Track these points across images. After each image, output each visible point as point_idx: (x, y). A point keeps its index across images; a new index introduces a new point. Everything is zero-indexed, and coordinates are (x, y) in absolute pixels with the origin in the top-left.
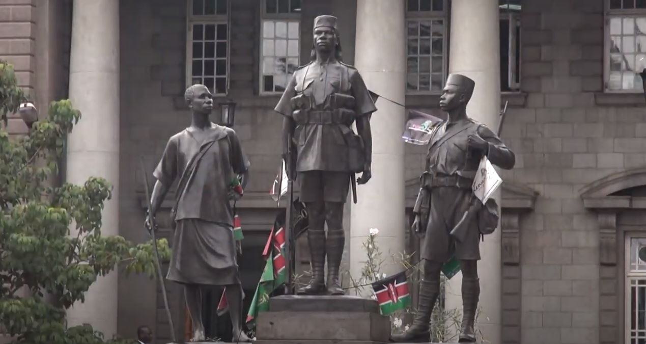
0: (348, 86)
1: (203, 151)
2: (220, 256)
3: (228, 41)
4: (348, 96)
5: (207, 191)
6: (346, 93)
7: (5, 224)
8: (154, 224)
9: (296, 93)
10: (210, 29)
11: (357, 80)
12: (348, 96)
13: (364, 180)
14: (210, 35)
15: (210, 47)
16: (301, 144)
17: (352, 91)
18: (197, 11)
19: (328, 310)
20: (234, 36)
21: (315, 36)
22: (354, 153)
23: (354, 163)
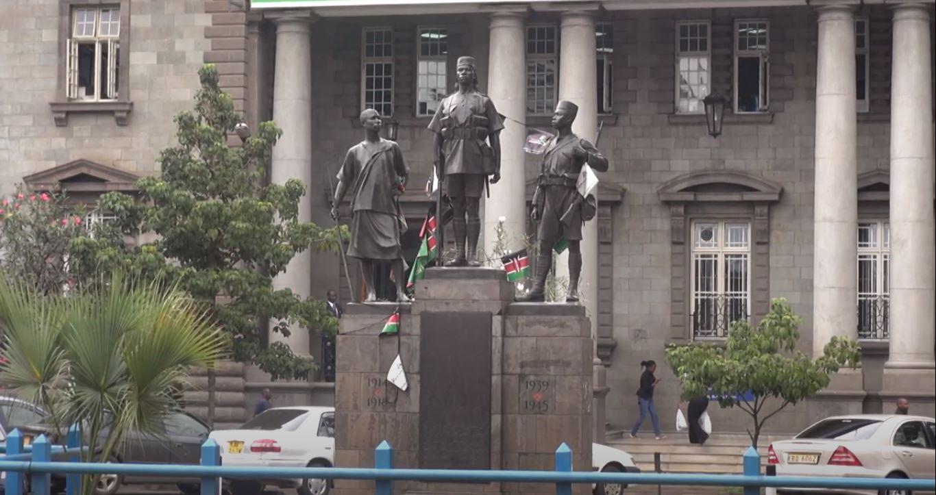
0: (483, 110)
1: (374, 159)
3: (392, 76)
4: (483, 117)
6: (481, 115)
8: (338, 213)
9: (444, 115)
10: (379, 67)
11: (489, 105)
12: (483, 117)
13: (495, 180)
14: (379, 72)
17: (486, 114)
21: (458, 72)
22: (487, 161)
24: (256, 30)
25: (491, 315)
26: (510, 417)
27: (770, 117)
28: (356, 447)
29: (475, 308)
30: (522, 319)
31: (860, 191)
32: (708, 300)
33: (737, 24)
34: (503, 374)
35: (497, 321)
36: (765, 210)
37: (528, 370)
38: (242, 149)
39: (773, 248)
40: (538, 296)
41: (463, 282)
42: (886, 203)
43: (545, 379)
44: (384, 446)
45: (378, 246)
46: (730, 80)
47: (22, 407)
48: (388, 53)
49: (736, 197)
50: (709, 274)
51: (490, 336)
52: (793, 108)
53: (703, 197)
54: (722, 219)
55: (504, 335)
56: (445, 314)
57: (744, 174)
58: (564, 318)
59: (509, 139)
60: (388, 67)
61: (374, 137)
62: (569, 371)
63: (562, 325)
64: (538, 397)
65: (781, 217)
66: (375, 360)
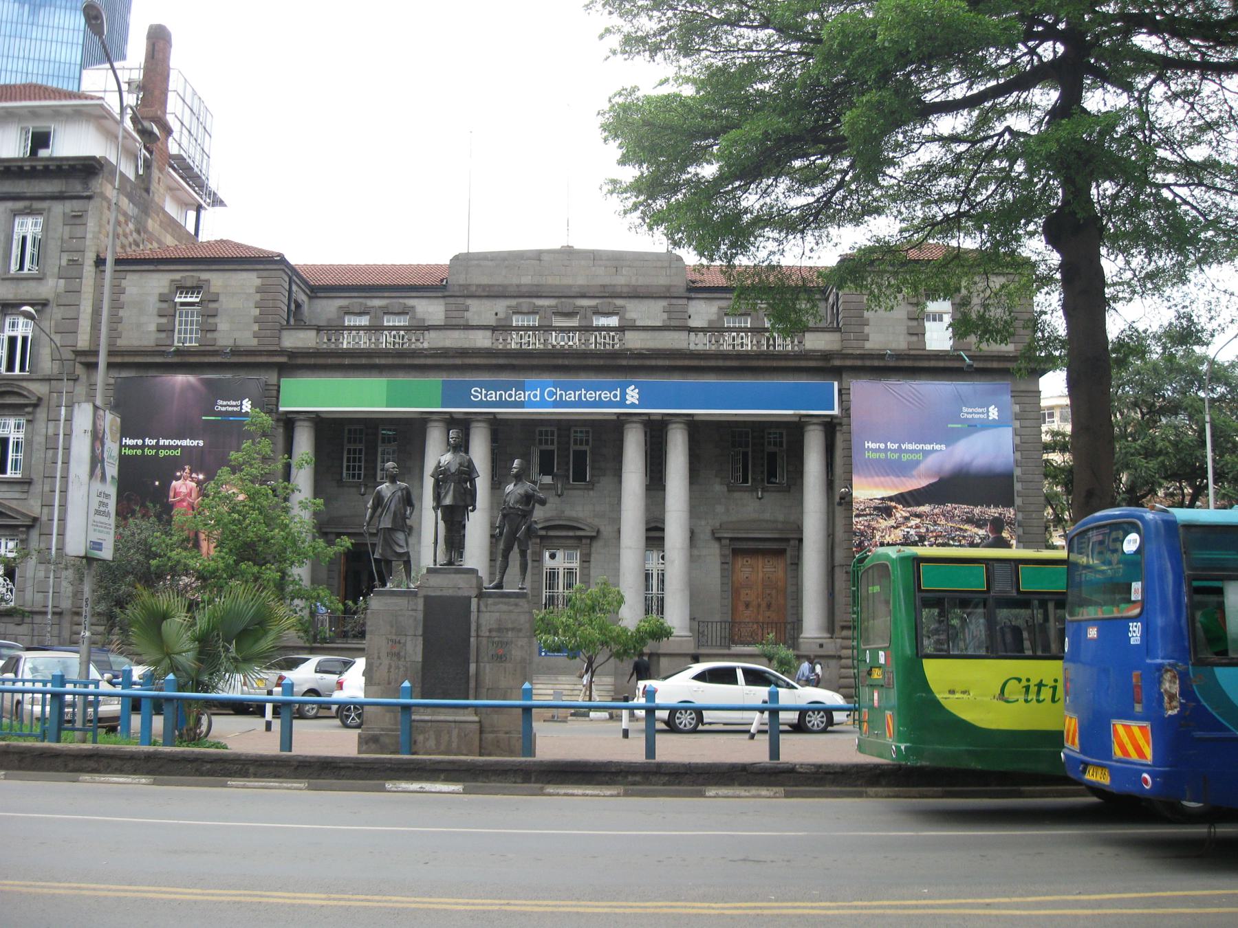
2: (401, 546)
3: (363, 456)
5: (395, 513)
7: (646, 632)
11: (470, 462)
13: (473, 510)
14: (355, 453)
15: (354, 467)
16: (443, 492)
17: (468, 467)
18: (349, 442)
19: (455, 573)
20: (366, 454)
22: (468, 498)
23: (469, 502)
24: (281, 424)
25: (470, 598)
26: (482, 664)
27: (591, 486)
28: (379, 684)
29: (460, 593)
30: (490, 601)
31: (648, 530)
32: (553, 596)
33: (572, 431)
34: (478, 636)
35: (474, 601)
36: (588, 541)
37: (494, 634)
38: (143, 547)
39: (593, 564)
40: (499, 586)
41: (453, 576)
42: (663, 539)
43: (505, 640)
44: (407, 684)
45: (396, 552)
46: (568, 463)
47: (398, 655)
48: (361, 442)
49: (571, 534)
50: (554, 580)
51: (469, 612)
52: (605, 482)
53: (551, 533)
54: (562, 547)
55: (478, 611)
56: (441, 596)
57: (576, 520)
58: (517, 600)
59: (482, 485)
60: (360, 450)
61: (393, 479)
62: (521, 635)
63: (516, 605)
64: (501, 652)
65: (597, 546)
66: (392, 626)
